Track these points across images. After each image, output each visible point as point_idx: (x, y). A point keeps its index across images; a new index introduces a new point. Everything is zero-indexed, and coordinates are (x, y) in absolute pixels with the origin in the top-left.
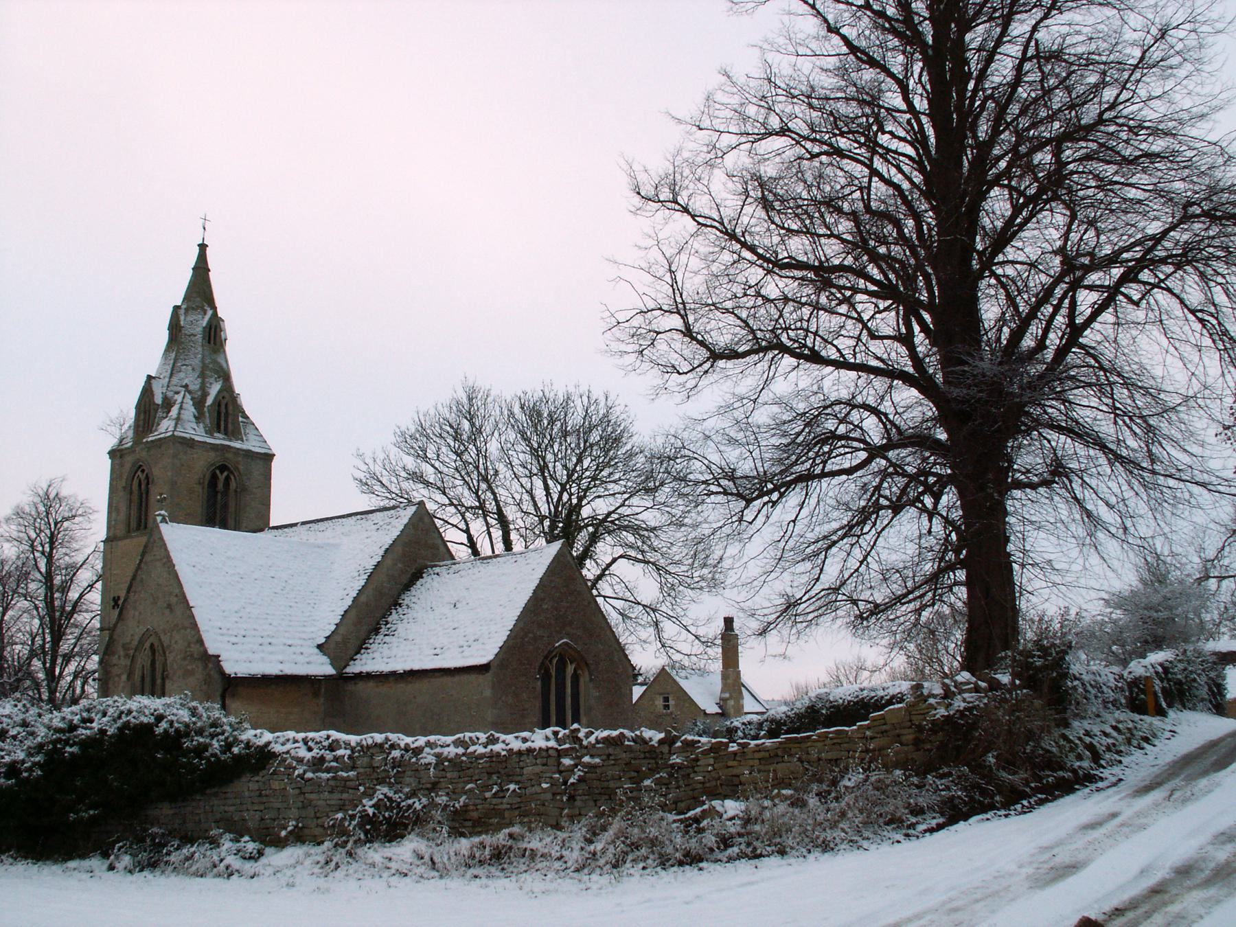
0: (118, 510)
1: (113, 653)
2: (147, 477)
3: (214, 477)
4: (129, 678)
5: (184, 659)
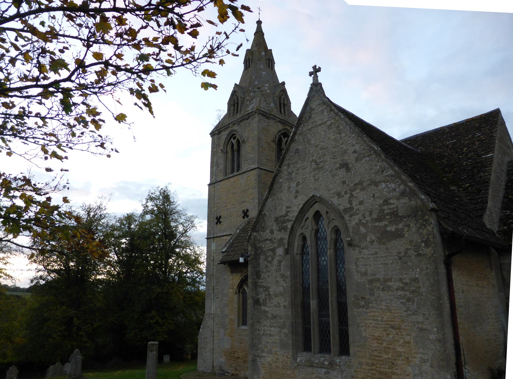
0: (218, 166)
1: (264, 229)
2: (238, 141)
3: (280, 140)
4: (287, 252)
5: (379, 219)
